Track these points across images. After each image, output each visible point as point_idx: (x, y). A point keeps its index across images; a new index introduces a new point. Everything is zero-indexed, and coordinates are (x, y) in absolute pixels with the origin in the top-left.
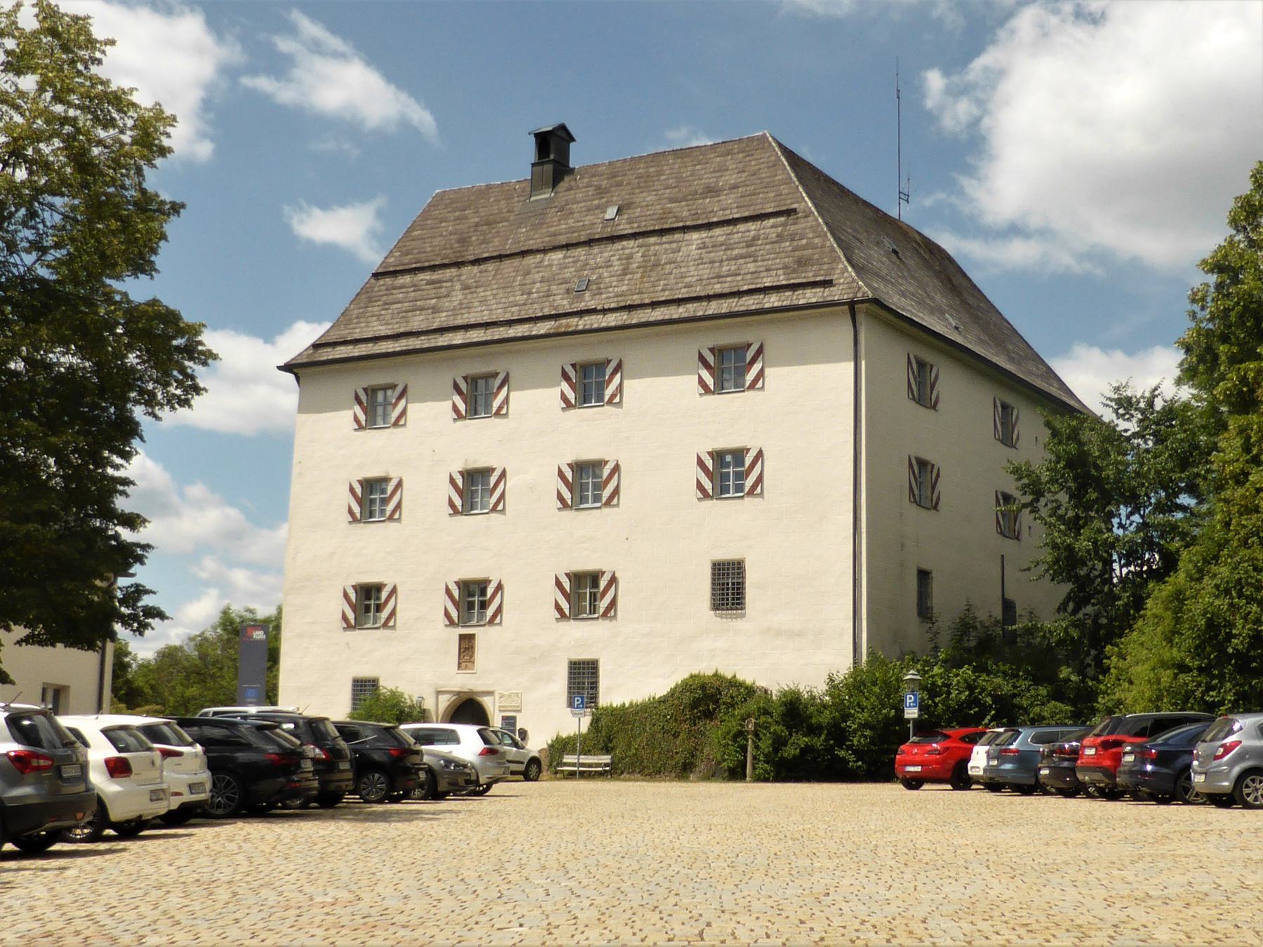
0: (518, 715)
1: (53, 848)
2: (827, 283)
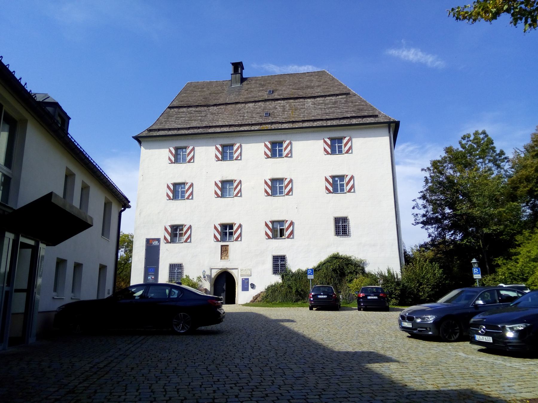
1: (200, 328)
2: (376, 116)
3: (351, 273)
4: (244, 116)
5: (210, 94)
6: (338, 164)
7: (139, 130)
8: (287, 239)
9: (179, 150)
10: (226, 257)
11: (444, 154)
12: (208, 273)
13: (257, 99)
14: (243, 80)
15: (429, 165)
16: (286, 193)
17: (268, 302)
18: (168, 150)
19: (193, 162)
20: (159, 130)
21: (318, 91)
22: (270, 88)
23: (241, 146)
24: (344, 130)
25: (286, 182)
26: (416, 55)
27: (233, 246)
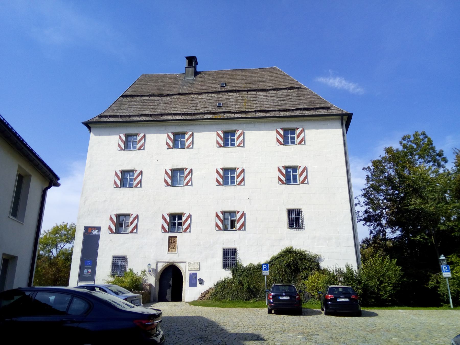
0: (197, 272)
2: (329, 109)
3: (306, 268)
4: (196, 106)
5: (164, 85)
6: (291, 155)
7: (91, 116)
8: (238, 231)
9: (129, 138)
10: (174, 250)
11: (383, 154)
12: (154, 266)
13: (210, 91)
14: (196, 73)
15: (370, 164)
16: (238, 183)
17: (217, 300)
18: (118, 136)
19: (144, 149)
20: (110, 116)
21: (270, 85)
22: (223, 81)
23: (193, 135)
24: (296, 121)
25: (238, 172)
26: (341, 82)
27: (182, 238)
